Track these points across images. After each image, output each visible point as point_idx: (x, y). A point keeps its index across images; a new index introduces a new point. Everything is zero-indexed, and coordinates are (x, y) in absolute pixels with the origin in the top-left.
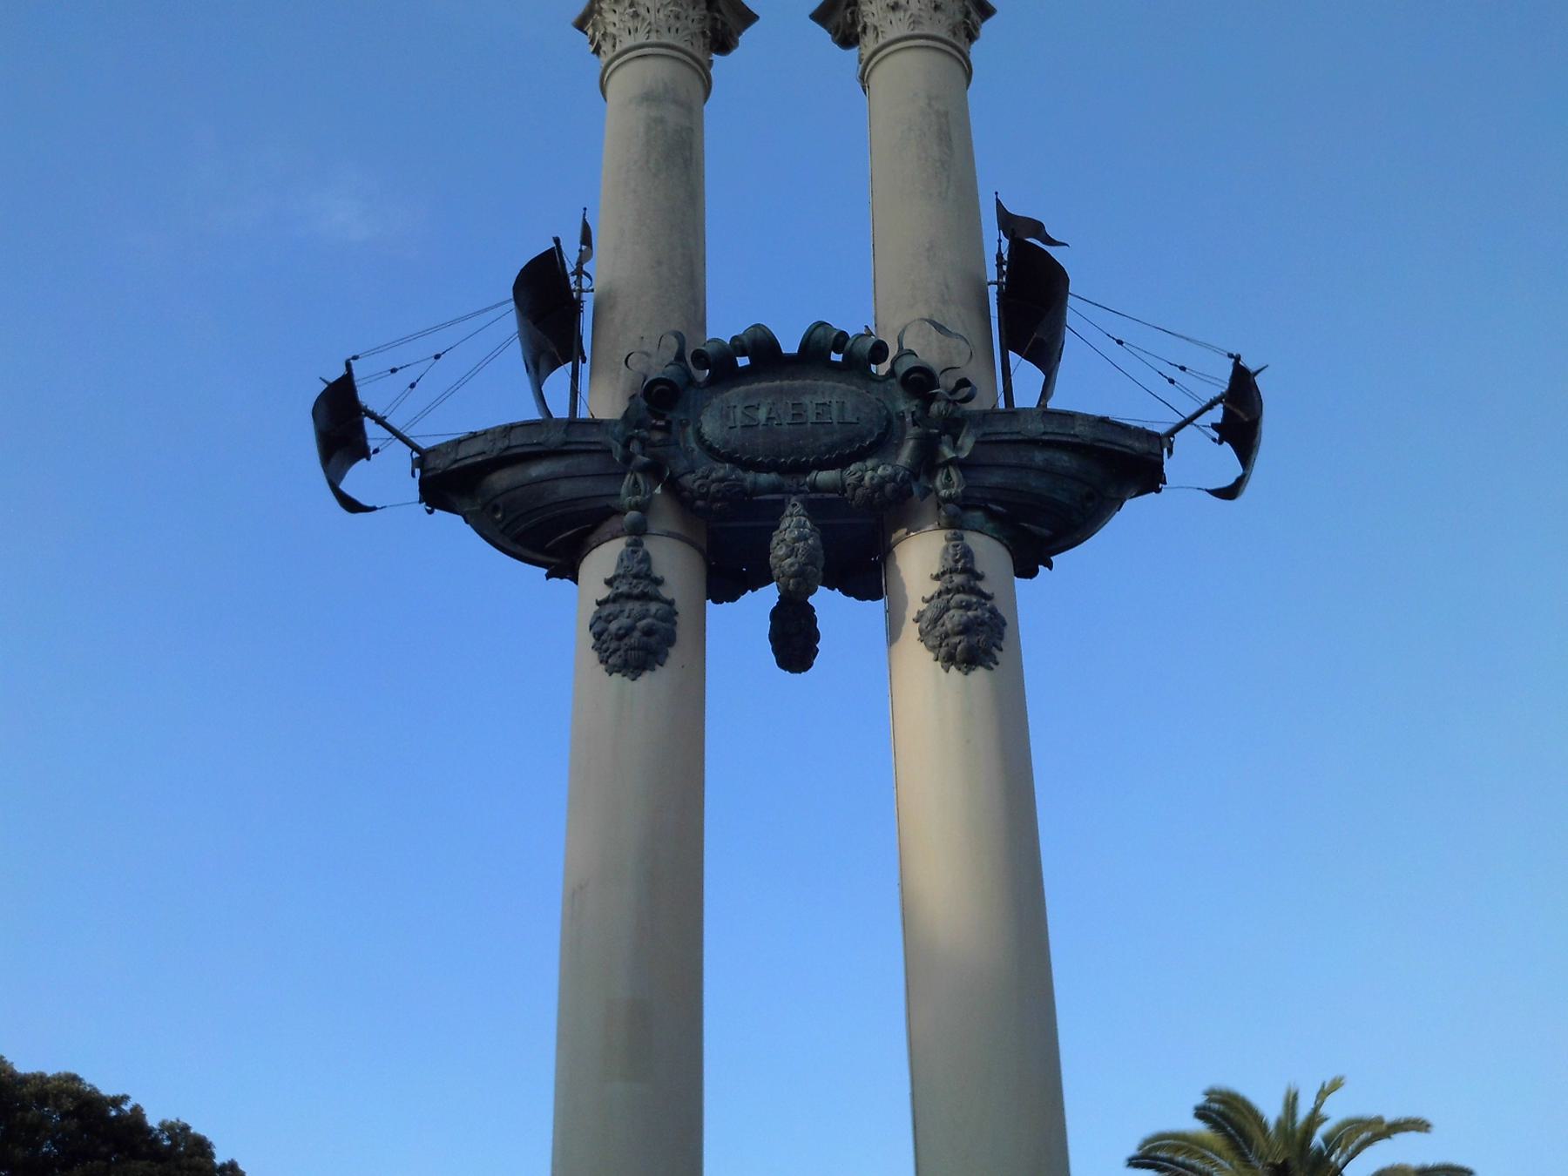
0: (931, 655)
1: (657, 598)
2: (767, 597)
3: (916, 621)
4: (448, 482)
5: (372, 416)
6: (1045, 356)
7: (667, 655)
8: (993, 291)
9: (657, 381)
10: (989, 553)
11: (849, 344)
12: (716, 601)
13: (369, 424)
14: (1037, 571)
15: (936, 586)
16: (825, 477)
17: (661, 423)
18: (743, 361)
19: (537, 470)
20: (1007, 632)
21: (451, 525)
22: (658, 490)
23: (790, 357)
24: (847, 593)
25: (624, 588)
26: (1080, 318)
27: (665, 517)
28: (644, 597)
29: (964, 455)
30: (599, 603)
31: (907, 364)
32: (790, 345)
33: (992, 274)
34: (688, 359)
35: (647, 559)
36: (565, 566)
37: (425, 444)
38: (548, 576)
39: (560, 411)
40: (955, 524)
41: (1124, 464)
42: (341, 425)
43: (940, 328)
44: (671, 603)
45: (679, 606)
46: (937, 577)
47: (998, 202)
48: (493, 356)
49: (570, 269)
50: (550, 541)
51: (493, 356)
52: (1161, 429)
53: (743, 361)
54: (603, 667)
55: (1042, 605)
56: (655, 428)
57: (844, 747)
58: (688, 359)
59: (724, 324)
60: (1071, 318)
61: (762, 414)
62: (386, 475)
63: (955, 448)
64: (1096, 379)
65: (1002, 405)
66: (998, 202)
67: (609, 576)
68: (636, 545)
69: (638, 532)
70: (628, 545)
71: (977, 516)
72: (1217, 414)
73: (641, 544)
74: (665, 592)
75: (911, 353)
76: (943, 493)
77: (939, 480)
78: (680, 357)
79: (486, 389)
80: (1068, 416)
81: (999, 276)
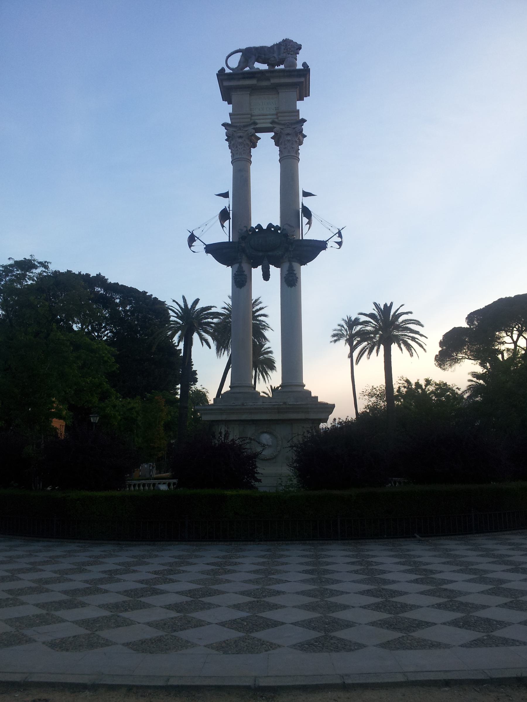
4: (211, 249)
10: (245, 266)
16: (270, 253)
18: (257, 230)
32: (265, 227)
37: (207, 243)
40: (290, 261)
41: (319, 246)
42: (192, 239)
57: (265, 213)
59: (254, 225)
62: (198, 246)
64: (310, 233)
66: (314, 195)
68: (240, 265)
69: (240, 263)
78: (247, 230)
79: (222, 235)
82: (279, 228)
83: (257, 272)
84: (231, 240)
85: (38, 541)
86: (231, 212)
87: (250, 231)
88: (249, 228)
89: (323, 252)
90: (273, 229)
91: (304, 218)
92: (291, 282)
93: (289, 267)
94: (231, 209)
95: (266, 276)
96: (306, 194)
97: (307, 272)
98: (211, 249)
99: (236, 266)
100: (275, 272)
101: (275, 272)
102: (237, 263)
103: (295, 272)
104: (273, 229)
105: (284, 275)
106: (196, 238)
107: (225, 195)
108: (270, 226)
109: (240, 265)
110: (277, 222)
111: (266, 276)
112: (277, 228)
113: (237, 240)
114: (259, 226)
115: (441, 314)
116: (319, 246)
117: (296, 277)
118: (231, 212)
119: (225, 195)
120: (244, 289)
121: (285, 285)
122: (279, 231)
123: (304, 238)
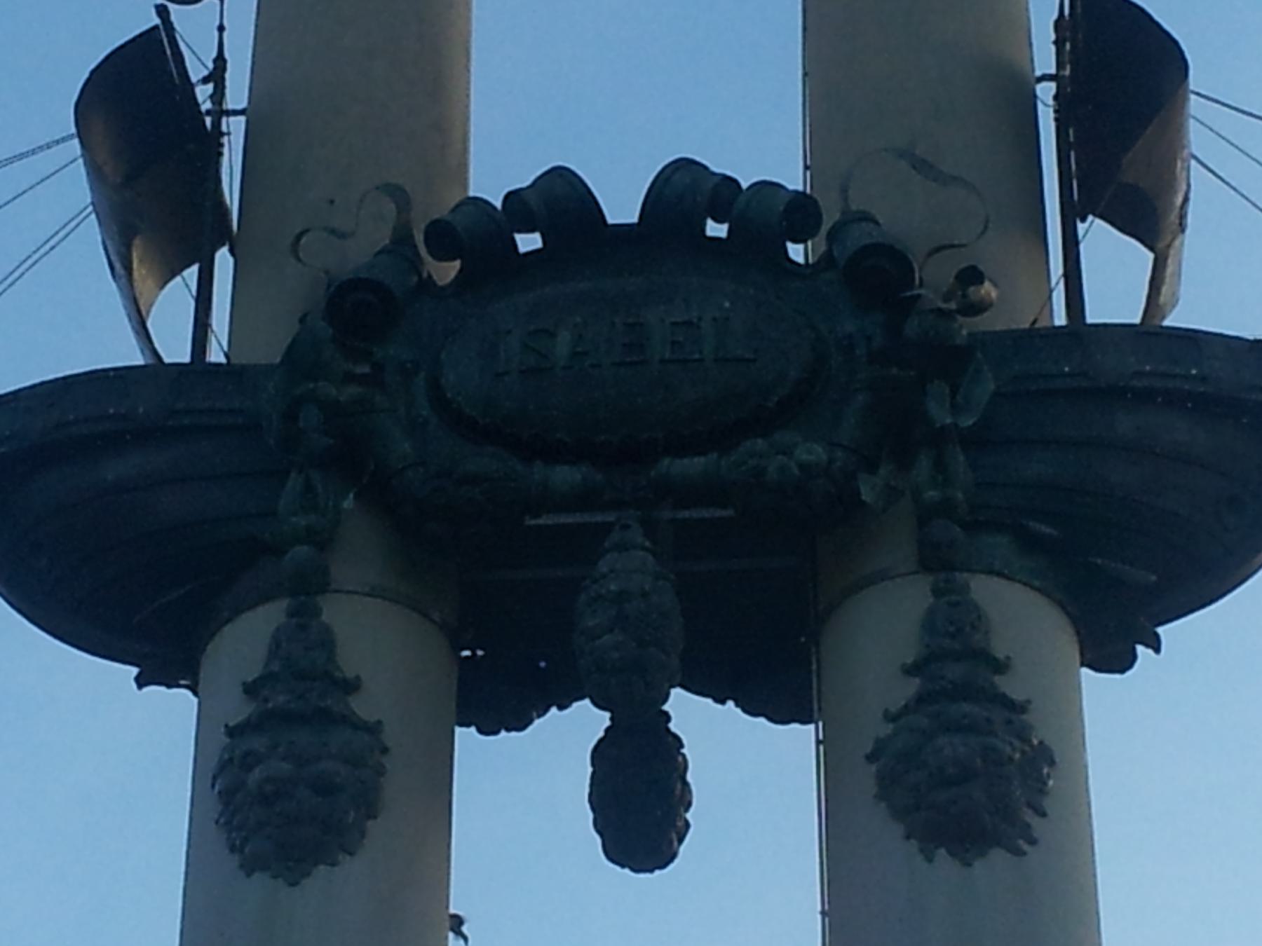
0: (898, 830)
1: (350, 722)
2: (581, 724)
3: (870, 758)
6: (1148, 215)
7: (363, 834)
8: (1046, 91)
9: (354, 284)
10: (380, 644)
11: (742, 199)
12: (487, 729)
14: (1133, 658)
15: (913, 686)
17: (365, 369)
18: (529, 242)
19: (114, 469)
22: (348, 503)
23: (623, 230)
24: (751, 709)
26: (1206, 131)
27: (360, 553)
29: (967, 422)
30: (231, 732)
31: (859, 237)
32: (622, 206)
33: (1045, 58)
34: (419, 238)
35: (327, 643)
38: (141, 682)
39: (176, 350)
40: (937, 561)
43: (922, 166)
44: (374, 729)
45: (390, 736)
46: (911, 670)
48: (48, 246)
49: (196, 72)
50: (129, 606)
51: (48, 246)
53: (529, 242)
54: (236, 859)
56: (350, 378)
58: (419, 238)
59: (496, 169)
60: (1197, 139)
61: (563, 344)
63: (955, 409)
65: (1060, 319)
68: (303, 615)
69: (307, 588)
70: (291, 614)
71: (1000, 545)
73: (317, 612)
74: (362, 707)
75: (866, 217)
76: (932, 494)
77: (923, 466)
78: (402, 238)
80: (1194, 341)
81: (1060, 65)
82: (799, 213)
83: (520, 788)
84: (216, 355)
86: (235, 128)
87: (443, 238)
88: (443, 206)
90: (716, 229)
91: (1098, 236)
92: (960, 802)
93: (929, 625)
94: (237, 96)
95: (640, 810)
100: (753, 773)
101: (753, 773)
102: (266, 598)
103: (1010, 686)
109: (303, 615)
110: (765, 145)
111: (640, 810)
112: (768, 217)
113: (269, 350)
114: (560, 201)
117: (1023, 734)
118: (235, 128)
120: (340, 888)
121: (886, 837)
122: (796, 252)
123: (1094, 315)
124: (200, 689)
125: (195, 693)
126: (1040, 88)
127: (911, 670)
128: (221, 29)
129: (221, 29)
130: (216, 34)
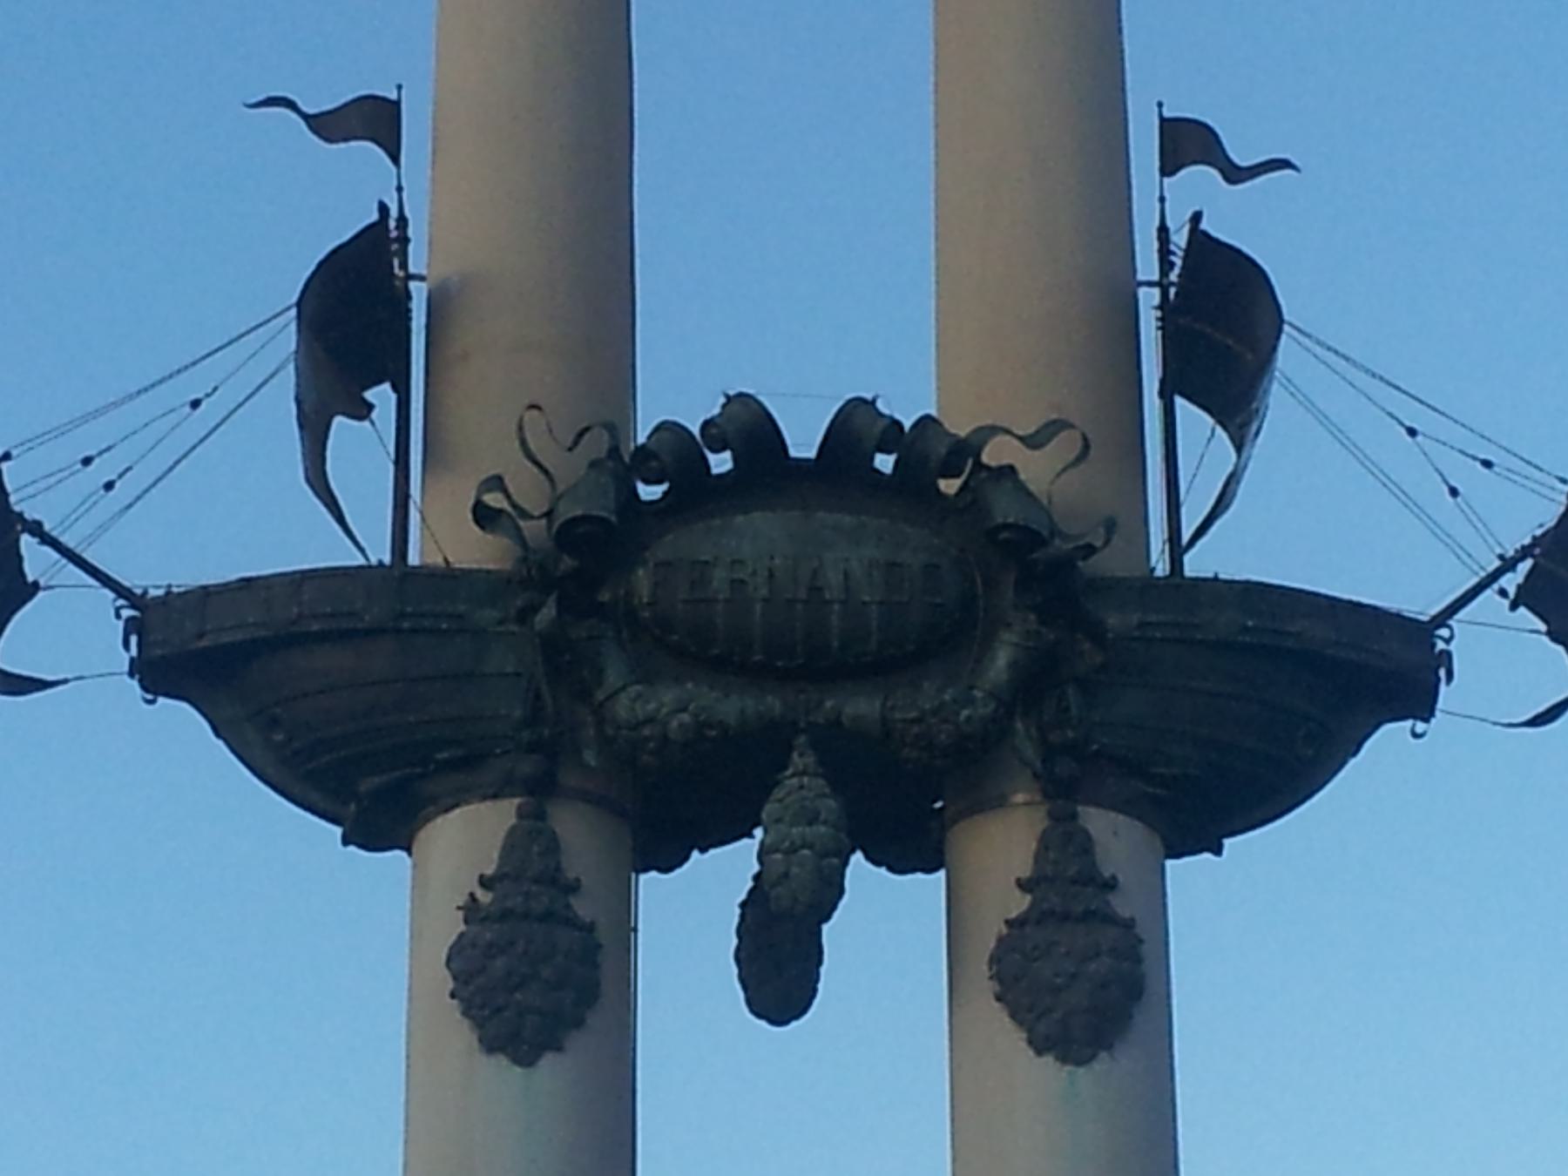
1: (1110, 919)
4: (199, 651)
5: (36, 529)
8: (1149, 298)
10: (580, 835)
13: (27, 542)
18: (721, 462)
20: (453, 926)
21: (181, 719)
25: (515, 902)
28: (547, 917)
32: (803, 439)
36: (379, 822)
38: (346, 841)
40: (1062, 794)
41: (1371, 671)
44: (590, 928)
47: (395, 159)
50: (364, 785)
52: (1422, 607)
55: (1221, 910)
57: (805, 279)
59: (674, 390)
62: (69, 629)
64: (1284, 510)
65: (1161, 568)
66: (395, 159)
67: (489, 871)
68: (533, 816)
70: (521, 814)
72: (1511, 581)
79: (259, 505)
83: (687, 915)
84: (413, 559)
85: (1266, 392)
87: (646, 462)
89: (1391, 737)
90: (885, 462)
92: (1076, 989)
95: (779, 965)
96: (1187, 143)
97: (1233, 920)
98: (199, 651)
99: (468, 837)
103: (1122, 905)
104: (885, 462)
105: (988, 932)
106: (35, 558)
107: (375, 120)
108: (855, 427)
111: (779, 965)
112: (926, 449)
115: (1452, 647)
116: (1371, 671)
119: (375, 120)
124: (414, 850)
125: (410, 854)
126: (1142, 291)
127: (1022, 885)
128: (1162, 199)
129: (1162, 199)
130: (1157, 205)
